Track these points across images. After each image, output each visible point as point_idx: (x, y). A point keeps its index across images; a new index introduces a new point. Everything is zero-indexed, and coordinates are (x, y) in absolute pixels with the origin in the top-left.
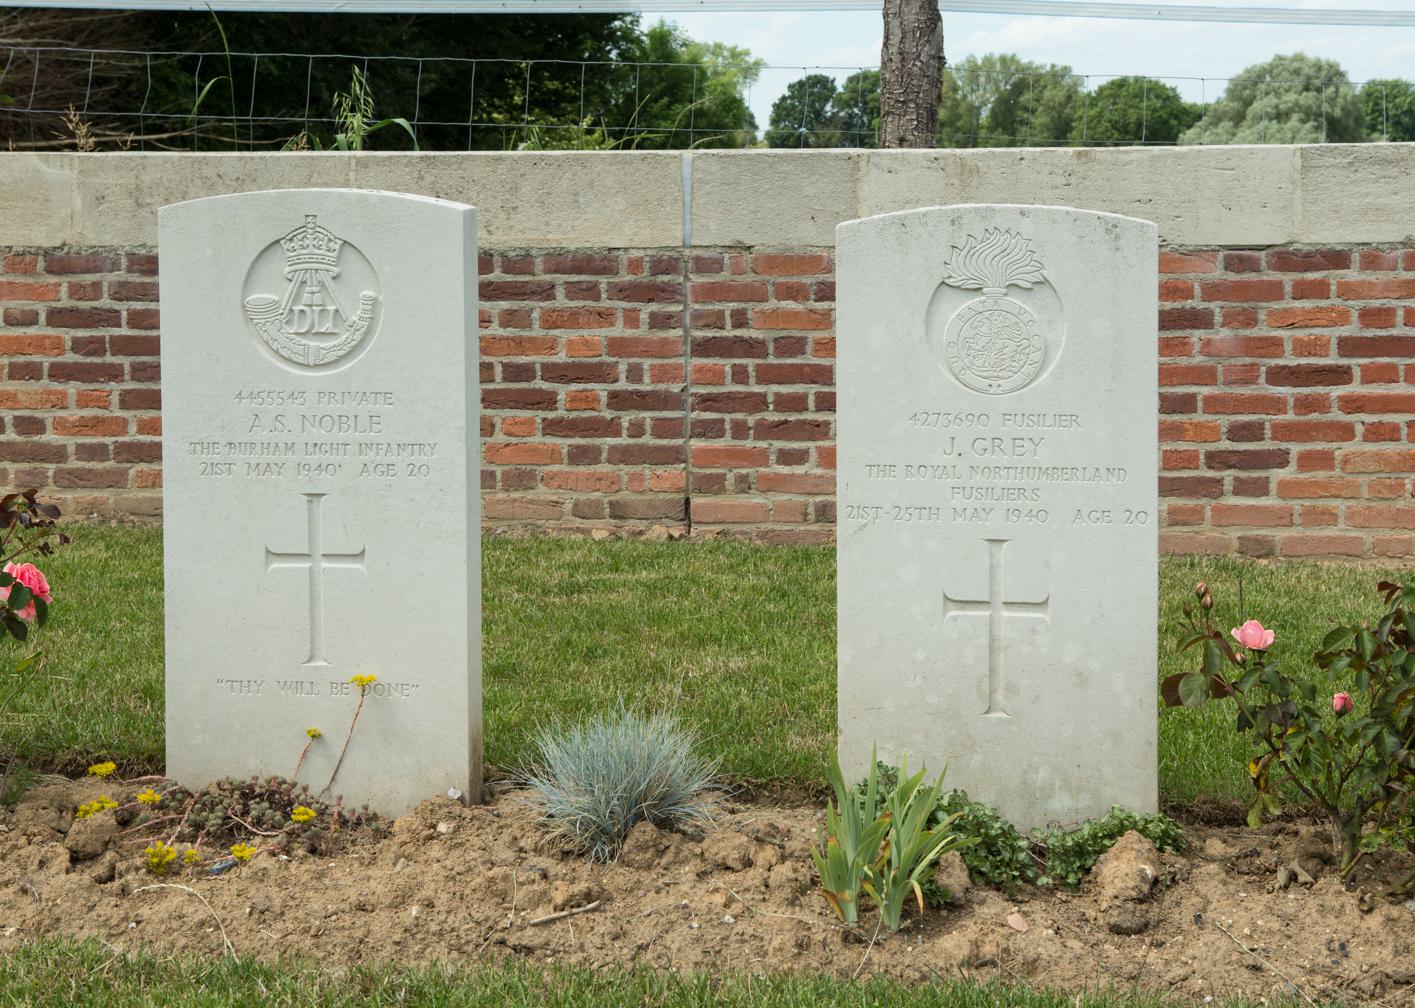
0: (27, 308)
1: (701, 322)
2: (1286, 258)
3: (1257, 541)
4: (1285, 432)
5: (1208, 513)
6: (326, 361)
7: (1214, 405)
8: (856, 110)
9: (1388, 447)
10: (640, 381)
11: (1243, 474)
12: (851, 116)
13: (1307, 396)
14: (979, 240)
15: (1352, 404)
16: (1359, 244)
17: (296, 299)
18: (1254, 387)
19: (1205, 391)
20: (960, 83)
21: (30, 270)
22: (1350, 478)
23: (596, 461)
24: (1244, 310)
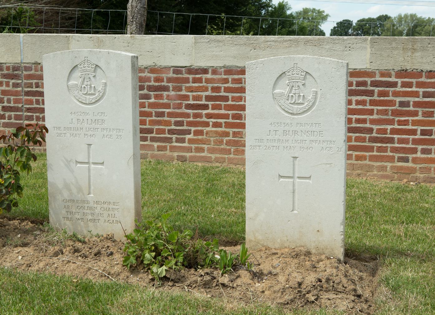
1: (27, 86)
2: (190, 70)
3: (182, 156)
4: (190, 124)
5: (168, 148)
6: (92, 102)
7: (170, 115)
8: (359, 32)
9: (219, 129)
10: (10, 103)
11: (178, 136)
13: (196, 113)
15: (209, 116)
16: (211, 67)
17: (290, 92)
18: (181, 110)
19: (168, 110)
22: (208, 138)
24: (179, 86)
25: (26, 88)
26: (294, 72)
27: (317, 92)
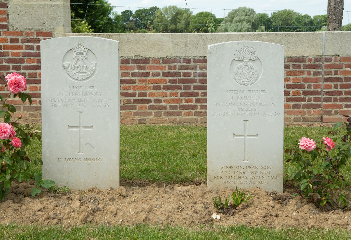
0: (157, 72)
8: (138, 19)
10: (311, 88)
12: (136, 20)
14: (243, 49)
17: (76, 64)
20: (163, 12)
21: (159, 63)
23: (299, 108)
25: (325, 75)
26: (79, 49)
27: (96, 64)
